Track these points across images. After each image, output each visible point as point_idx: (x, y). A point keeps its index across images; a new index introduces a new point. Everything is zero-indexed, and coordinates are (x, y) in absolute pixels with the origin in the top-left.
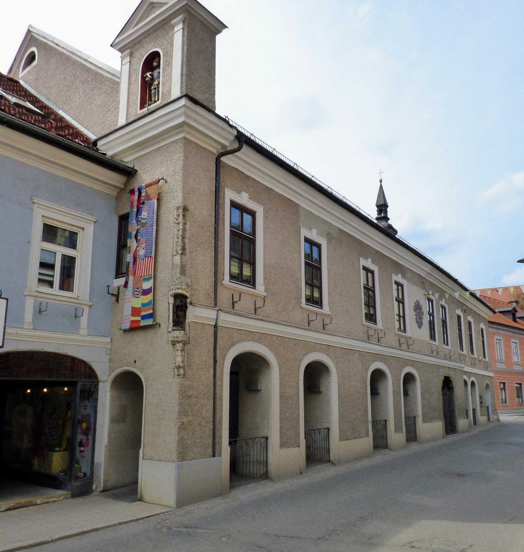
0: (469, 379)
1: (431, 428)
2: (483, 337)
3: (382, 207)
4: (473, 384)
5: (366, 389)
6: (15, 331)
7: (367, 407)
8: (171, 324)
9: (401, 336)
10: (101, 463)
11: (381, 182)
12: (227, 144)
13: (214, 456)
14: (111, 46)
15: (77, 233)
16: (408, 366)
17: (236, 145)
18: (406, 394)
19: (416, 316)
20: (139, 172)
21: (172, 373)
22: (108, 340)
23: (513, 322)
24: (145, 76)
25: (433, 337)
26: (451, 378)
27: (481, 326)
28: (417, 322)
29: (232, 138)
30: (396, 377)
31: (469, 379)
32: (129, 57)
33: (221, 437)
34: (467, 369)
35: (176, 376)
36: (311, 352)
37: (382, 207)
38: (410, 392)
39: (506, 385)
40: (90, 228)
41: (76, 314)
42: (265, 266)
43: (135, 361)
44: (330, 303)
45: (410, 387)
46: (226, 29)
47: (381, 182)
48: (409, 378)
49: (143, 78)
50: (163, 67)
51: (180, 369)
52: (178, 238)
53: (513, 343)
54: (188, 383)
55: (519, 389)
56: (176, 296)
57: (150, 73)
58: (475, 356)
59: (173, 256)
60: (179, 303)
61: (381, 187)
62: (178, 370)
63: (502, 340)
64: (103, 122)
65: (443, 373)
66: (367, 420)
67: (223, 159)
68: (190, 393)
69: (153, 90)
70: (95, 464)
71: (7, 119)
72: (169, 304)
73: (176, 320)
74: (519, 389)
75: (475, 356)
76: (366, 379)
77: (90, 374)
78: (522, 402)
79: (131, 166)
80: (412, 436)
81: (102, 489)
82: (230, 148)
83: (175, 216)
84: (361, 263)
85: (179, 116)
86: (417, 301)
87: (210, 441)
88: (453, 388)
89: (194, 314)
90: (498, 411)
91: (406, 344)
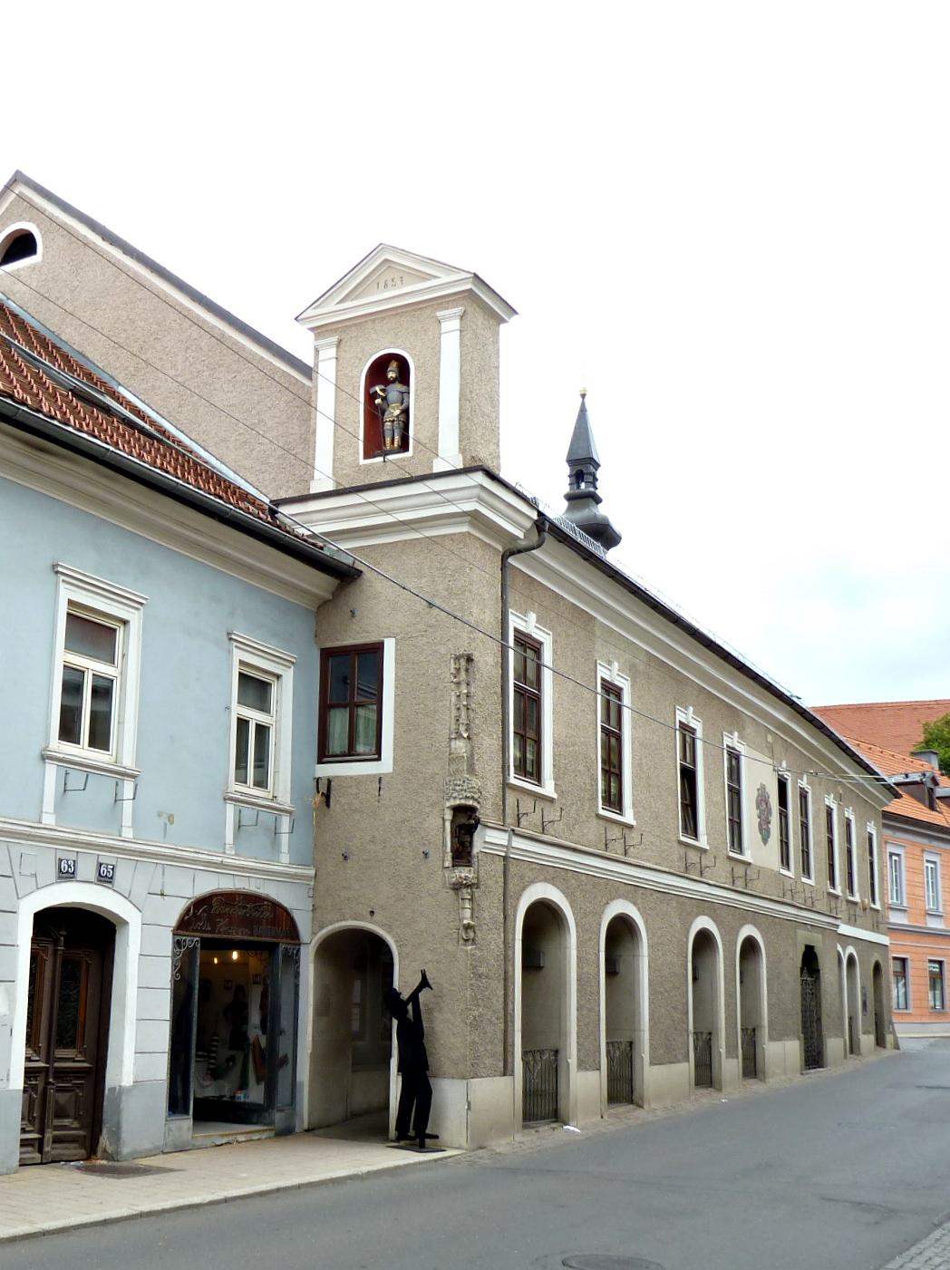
0: (844, 949)
1: (783, 1052)
2: (871, 853)
3: (583, 468)
4: (851, 960)
5: (686, 970)
6: (220, 859)
7: (687, 1004)
8: (449, 856)
9: (687, 845)
10: (303, 1082)
11: (583, 396)
12: (520, 534)
13: (504, 1075)
14: (296, 319)
15: (271, 684)
16: (748, 923)
17: (535, 538)
18: (612, 972)
19: (759, 817)
20: (367, 574)
21: (455, 935)
22: (312, 872)
23: (928, 811)
24: (372, 391)
25: (785, 861)
26: (817, 950)
27: (727, 741)
28: (761, 830)
29: (528, 524)
30: (729, 945)
31: (844, 949)
32: (335, 349)
33: (513, 1045)
34: (844, 929)
35: (461, 942)
36: (614, 899)
37: (583, 468)
38: (622, 968)
39: (910, 964)
40: (288, 675)
41: (240, 821)
42: (555, 743)
43: (372, 912)
44: (634, 805)
45: (624, 954)
46: (516, 317)
47: (583, 396)
48: (621, 931)
49: (370, 397)
50: (416, 390)
51: (469, 931)
52: (459, 709)
53: (928, 861)
54: (478, 953)
55: (936, 980)
56: (457, 810)
57: (383, 387)
58: (703, 842)
59: (451, 739)
60: (463, 820)
61: (583, 410)
62: (466, 932)
63: (903, 857)
64: (245, 442)
65: (804, 937)
66: (687, 1030)
67: (511, 560)
68: (482, 970)
69: (389, 424)
70: (298, 1084)
71: (232, 515)
72: (444, 820)
73: (458, 849)
74: (936, 980)
75: (857, 898)
76: (687, 949)
77: (292, 932)
78: (943, 1007)
79: (349, 561)
80: (622, 1089)
81: (306, 1126)
82: (523, 544)
83: (453, 671)
84: (677, 716)
85: (468, 499)
86: (761, 784)
87: (500, 1049)
88: (818, 971)
89: (489, 839)
90: (896, 1026)
91: (742, 875)
